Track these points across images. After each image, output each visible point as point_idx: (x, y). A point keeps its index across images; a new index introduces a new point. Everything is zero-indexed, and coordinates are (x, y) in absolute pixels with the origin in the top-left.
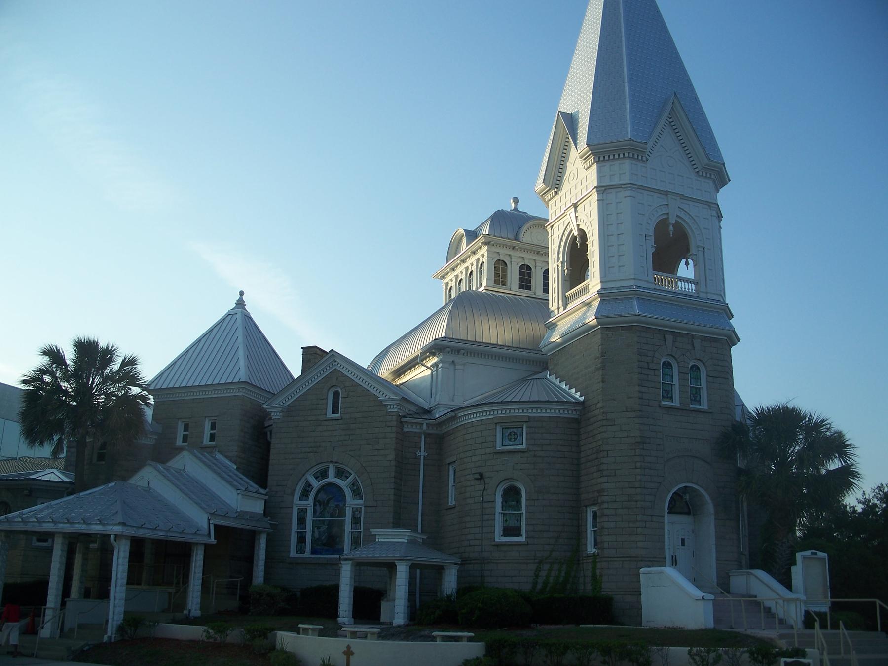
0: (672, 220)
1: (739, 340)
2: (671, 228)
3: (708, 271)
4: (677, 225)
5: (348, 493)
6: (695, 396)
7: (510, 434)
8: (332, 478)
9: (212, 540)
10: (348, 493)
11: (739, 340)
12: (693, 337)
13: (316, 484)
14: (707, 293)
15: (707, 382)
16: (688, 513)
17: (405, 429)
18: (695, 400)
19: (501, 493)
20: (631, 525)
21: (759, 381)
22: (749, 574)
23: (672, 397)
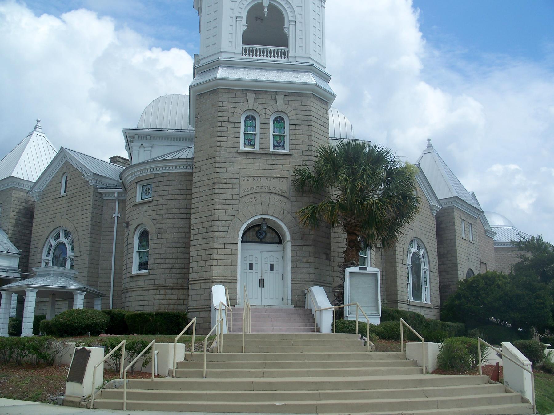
0: (266, 3)
2: (266, 10)
3: (297, 39)
4: (271, 7)
5: (69, 247)
7: (146, 190)
8: (62, 239)
10: (69, 247)
11: (335, 96)
13: (54, 243)
14: (295, 57)
17: (105, 198)
19: (138, 236)
20: (207, 252)
21: (344, 123)
23: (254, 145)
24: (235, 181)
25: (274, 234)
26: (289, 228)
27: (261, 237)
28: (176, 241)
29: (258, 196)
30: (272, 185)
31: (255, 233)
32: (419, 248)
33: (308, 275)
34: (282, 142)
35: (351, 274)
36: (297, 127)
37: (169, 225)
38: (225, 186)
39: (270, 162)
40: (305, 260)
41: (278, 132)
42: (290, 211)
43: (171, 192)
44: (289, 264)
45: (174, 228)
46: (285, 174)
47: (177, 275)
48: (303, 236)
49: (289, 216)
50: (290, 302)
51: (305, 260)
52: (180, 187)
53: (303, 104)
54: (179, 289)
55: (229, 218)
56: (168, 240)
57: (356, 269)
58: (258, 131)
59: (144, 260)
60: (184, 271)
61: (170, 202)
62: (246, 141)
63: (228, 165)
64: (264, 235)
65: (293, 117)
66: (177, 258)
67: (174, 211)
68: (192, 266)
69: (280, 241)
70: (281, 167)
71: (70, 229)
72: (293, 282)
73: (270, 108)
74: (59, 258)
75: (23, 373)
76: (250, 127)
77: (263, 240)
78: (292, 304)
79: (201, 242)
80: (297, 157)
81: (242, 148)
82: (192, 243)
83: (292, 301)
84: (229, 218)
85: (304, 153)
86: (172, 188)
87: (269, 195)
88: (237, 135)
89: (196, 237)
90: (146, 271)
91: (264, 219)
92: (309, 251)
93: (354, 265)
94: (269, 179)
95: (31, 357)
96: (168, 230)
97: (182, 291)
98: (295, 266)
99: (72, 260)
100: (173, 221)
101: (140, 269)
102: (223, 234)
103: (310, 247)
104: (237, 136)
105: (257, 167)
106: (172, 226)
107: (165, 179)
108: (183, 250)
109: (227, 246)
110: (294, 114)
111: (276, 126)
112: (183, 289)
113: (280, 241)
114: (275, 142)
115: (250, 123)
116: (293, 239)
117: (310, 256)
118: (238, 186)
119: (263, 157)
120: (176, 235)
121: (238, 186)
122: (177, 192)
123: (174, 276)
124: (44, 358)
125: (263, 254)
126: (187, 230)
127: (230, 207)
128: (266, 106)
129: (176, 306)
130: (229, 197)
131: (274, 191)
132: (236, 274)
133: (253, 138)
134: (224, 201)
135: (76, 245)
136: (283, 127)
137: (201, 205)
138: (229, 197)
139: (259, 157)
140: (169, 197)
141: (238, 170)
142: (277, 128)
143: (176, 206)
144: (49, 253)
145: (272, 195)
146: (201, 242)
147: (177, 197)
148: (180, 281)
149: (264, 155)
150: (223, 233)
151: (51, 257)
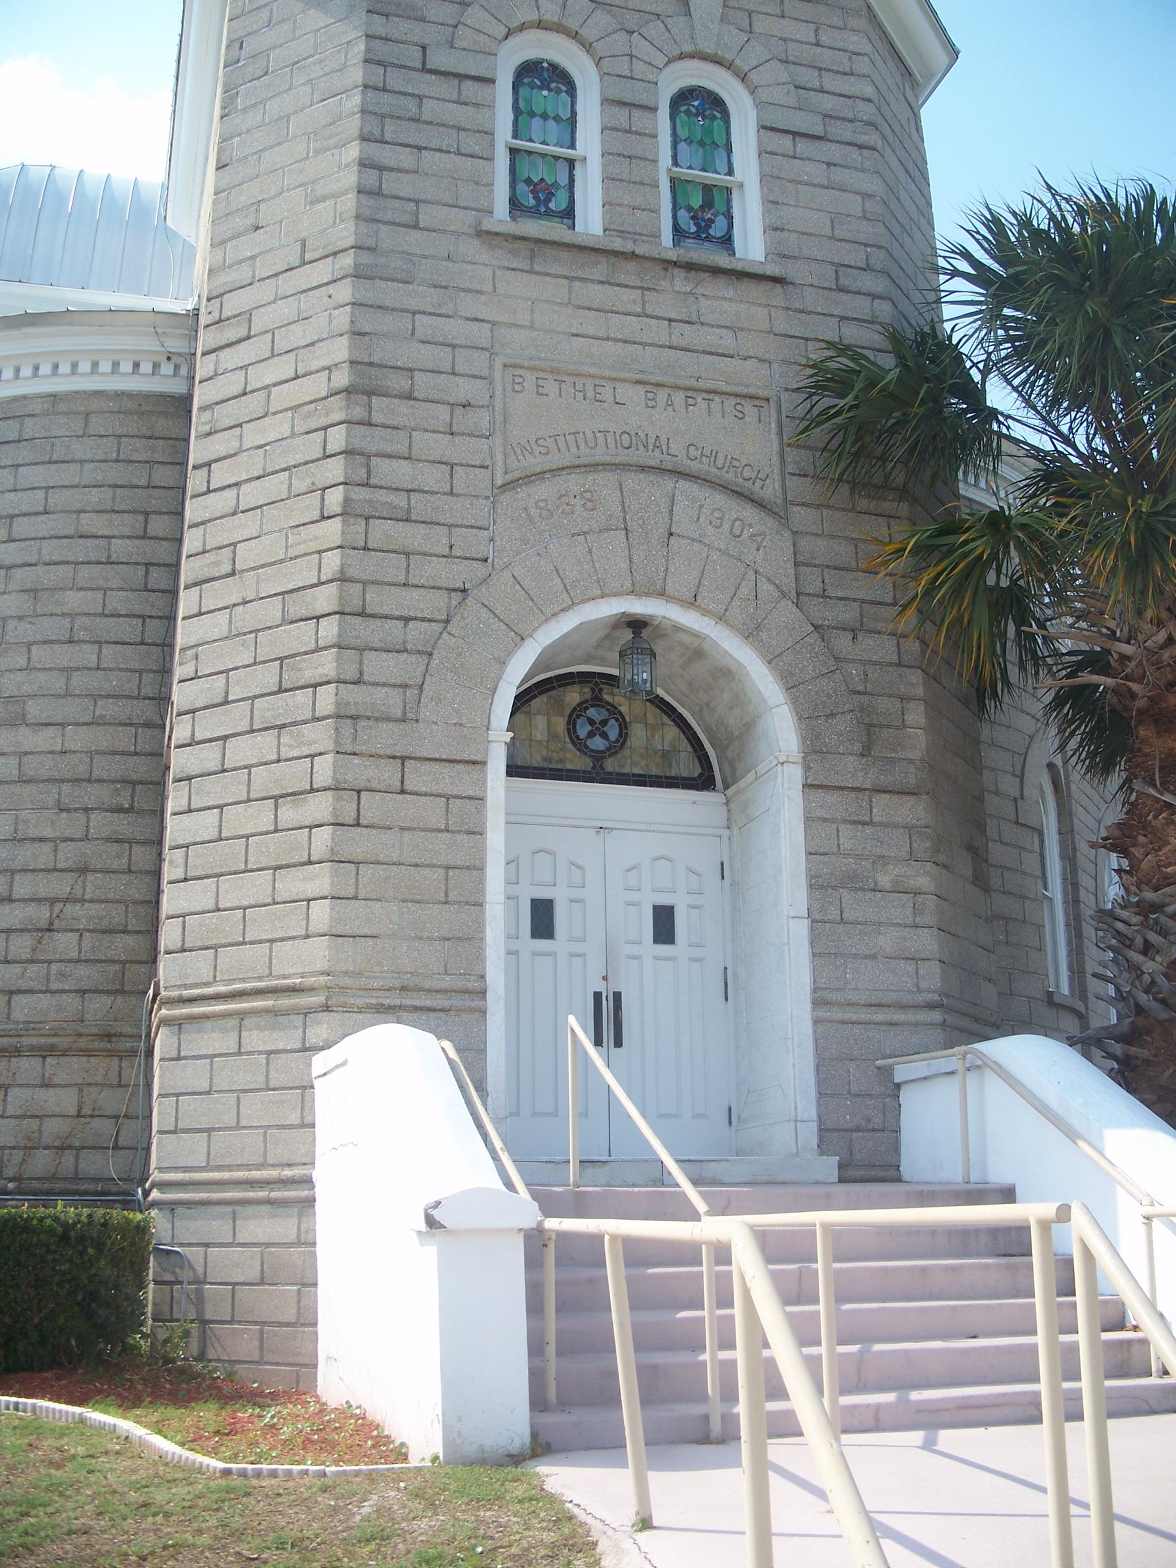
1: (954, 53)
15: (764, 153)
16: (704, 781)
18: (702, 233)
22: (979, 1066)
24: (463, 389)
25: (672, 732)
26: (791, 684)
27: (598, 743)
28: (82, 770)
29: (606, 484)
30: (685, 428)
31: (560, 724)
33: (910, 968)
34: (721, 222)
36: (803, 146)
37: (42, 677)
38: (403, 413)
39: (663, 304)
40: (884, 880)
41: (697, 162)
42: (789, 583)
43: (57, 499)
45: (67, 694)
46: (754, 377)
47: (82, 971)
48: (871, 735)
49: (787, 612)
50: (810, 1134)
51: (884, 880)
52: (114, 474)
53: (824, 39)
54: (88, 1053)
55: (435, 604)
56: (32, 766)
58: (590, 140)
60: (122, 946)
61: (50, 550)
62: (522, 188)
63: (426, 298)
64: (613, 734)
65: (779, 95)
66: (83, 870)
67: (74, 600)
68: (184, 906)
70: (727, 341)
72: (823, 1014)
73: (654, 29)
76: (545, 116)
77: (610, 765)
78: (823, 1147)
80: (811, 299)
82: (179, 761)
83: (827, 1134)
84: (435, 604)
85: (844, 282)
86: (68, 474)
87: (668, 483)
88: (471, 143)
89: (210, 725)
91: (637, 625)
92: (908, 828)
94: (662, 395)
96: (34, 710)
97: (104, 1068)
98: (834, 913)
100: (63, 656)
102: (393, 701)
103: (909, 801)
104: (476, 149)
105: (592, 323)
106: (59, 684)
107: (30, 428)
108: (123, 825)
109: (419, 777)
110: (784, 77)
111: (683, 133)
112: (111, 1053)
114: (683, 214)
115: (542, 99)
116: (815, 750)
117: (912, 857)
118: (483, 420)
119: (628, 272)
120: (78, 739)
121: (483, 420)
122: (95, 497)
123: (62, 975)
125: (622, 840)
126: (142, 710)
127: (438, 540)
128: (631, 20)
129: (69, 1158)
130: (432, 477)
131: (695, 466)
132: (480, 957)
133: (563, 180)
134: (400, 500)
136: (721, 141)
137: (248, 525)
138: (432, 477)
139: (601, 269)
140: (43, 526)
141: (481, 334)
142: (688, 140)
143: (85, 572)
145: (683, 484)
146: (241, 751)
147: (89, 523)
148: (97, 1006)
149: (631, 266)
150: (395, 697)
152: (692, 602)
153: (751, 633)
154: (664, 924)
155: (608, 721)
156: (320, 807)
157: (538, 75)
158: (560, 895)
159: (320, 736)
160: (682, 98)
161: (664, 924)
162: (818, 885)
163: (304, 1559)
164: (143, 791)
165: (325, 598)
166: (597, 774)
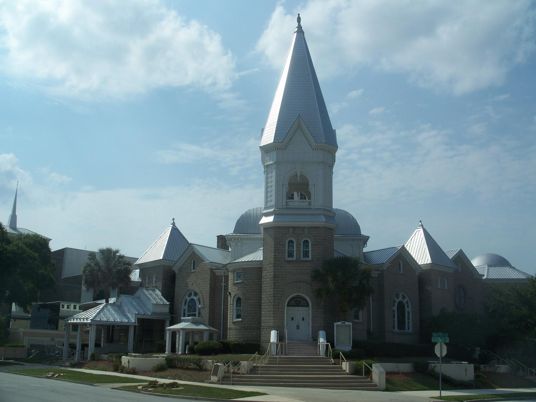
0: (299, 175)
5: (197, 302)
6: (306, 254)
8: (193, 297)
9: (137, 324)
12: (304, 228)
13: (188, 299)
26: (310, 299)
32: (404, 298)
35: (337, 325)
44: (311, 318)
57: (340, 323)
58: (295, 249)
59: (239, 313)
69: (307, 305)
71: (198, 292)
74: (192, 310)
75: (184, 371)
79: (267, 307)
81: (287, 259)
90: (240, 319)
93: (339, 321)
95: (193, 366)
99: (199, 309)
101: (237, 318)
113: (307, 305)
116: (313, 306)
124: (200, 366)
125: (299, 312)
135: (202, 301)
144: (185, 304)
151: (186, 307)
152: (302, 293)
153: (308, 296)
154: (303, 319)
155: (297, 302)
156: (272, 312)
157: (291, 242)
158: (294, 317)
159: (272, 307)
160: (304, 241)
161: (303, 319)
162: (313, 317)
163: (140, 23)
164: (260, 306)
165: (272, 295)
166: (298, 306)
